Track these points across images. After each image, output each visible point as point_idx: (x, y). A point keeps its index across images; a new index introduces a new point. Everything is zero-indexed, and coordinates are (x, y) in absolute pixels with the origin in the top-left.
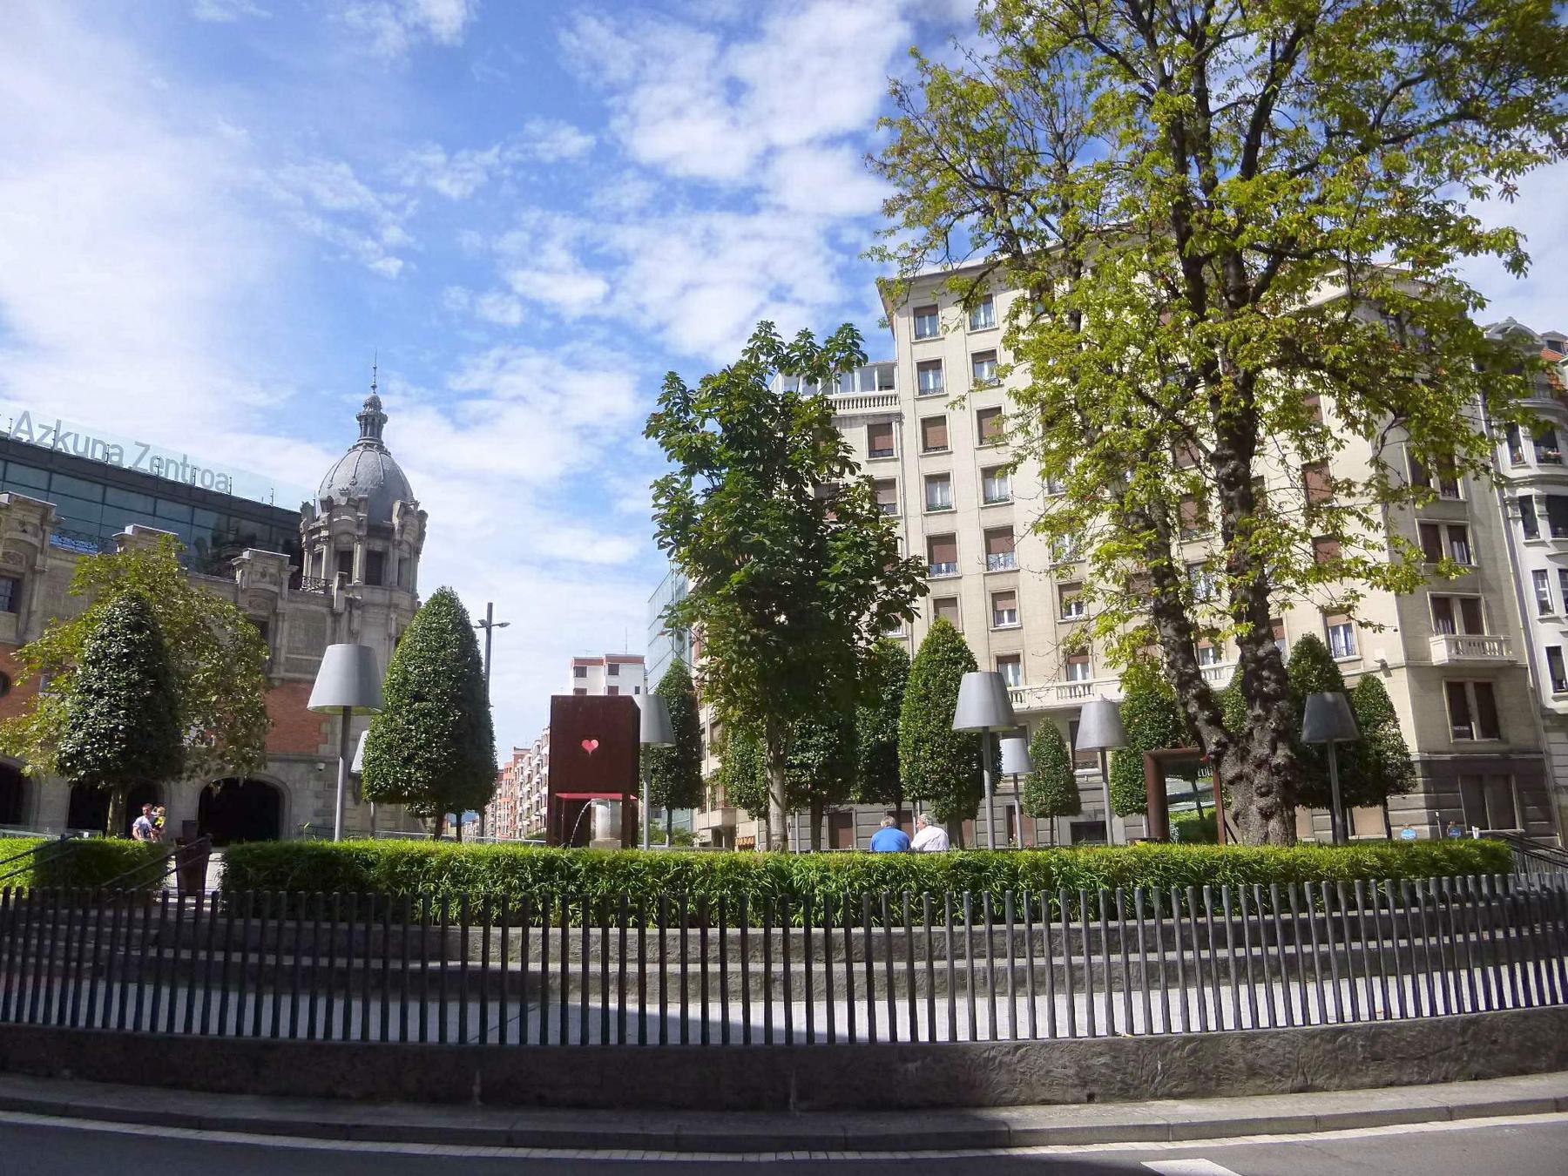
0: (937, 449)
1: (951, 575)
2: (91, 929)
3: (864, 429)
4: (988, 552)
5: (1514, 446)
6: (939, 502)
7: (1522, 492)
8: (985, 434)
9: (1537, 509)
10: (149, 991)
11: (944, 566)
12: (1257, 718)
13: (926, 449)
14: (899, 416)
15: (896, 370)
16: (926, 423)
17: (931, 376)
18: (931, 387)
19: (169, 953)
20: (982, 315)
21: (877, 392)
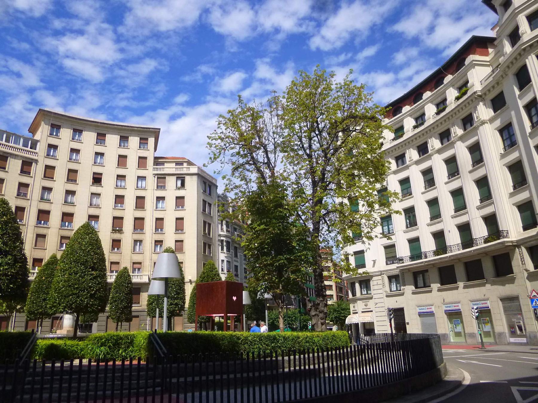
0: (49, 178)
1: (45, 226)
2: (110, 375)
3: (21, 161)
4: (62, 220)
5: (222, 225)
6: (46, 198)
7: (222, 238)
8: (69, 178)
9: (225, 243)
10: (257, 389)
11: (43, 222)
12: (321, 301)
13: (45, 177)
14: (36, 161)
15: (38, 144)
16: (47, 167)
17: (52, 151)
18: (52, 154)
19: (239, 375)
20: (77, 136)
21: (29, 149)
